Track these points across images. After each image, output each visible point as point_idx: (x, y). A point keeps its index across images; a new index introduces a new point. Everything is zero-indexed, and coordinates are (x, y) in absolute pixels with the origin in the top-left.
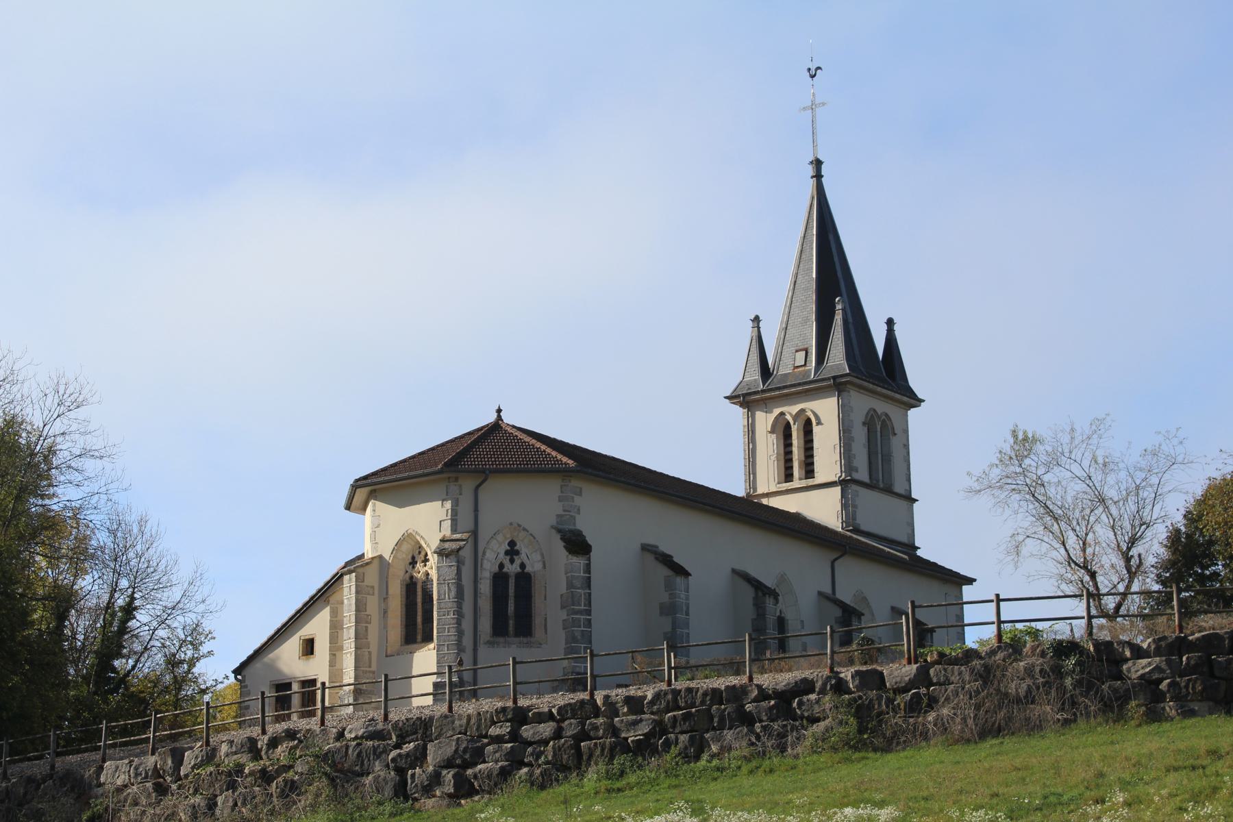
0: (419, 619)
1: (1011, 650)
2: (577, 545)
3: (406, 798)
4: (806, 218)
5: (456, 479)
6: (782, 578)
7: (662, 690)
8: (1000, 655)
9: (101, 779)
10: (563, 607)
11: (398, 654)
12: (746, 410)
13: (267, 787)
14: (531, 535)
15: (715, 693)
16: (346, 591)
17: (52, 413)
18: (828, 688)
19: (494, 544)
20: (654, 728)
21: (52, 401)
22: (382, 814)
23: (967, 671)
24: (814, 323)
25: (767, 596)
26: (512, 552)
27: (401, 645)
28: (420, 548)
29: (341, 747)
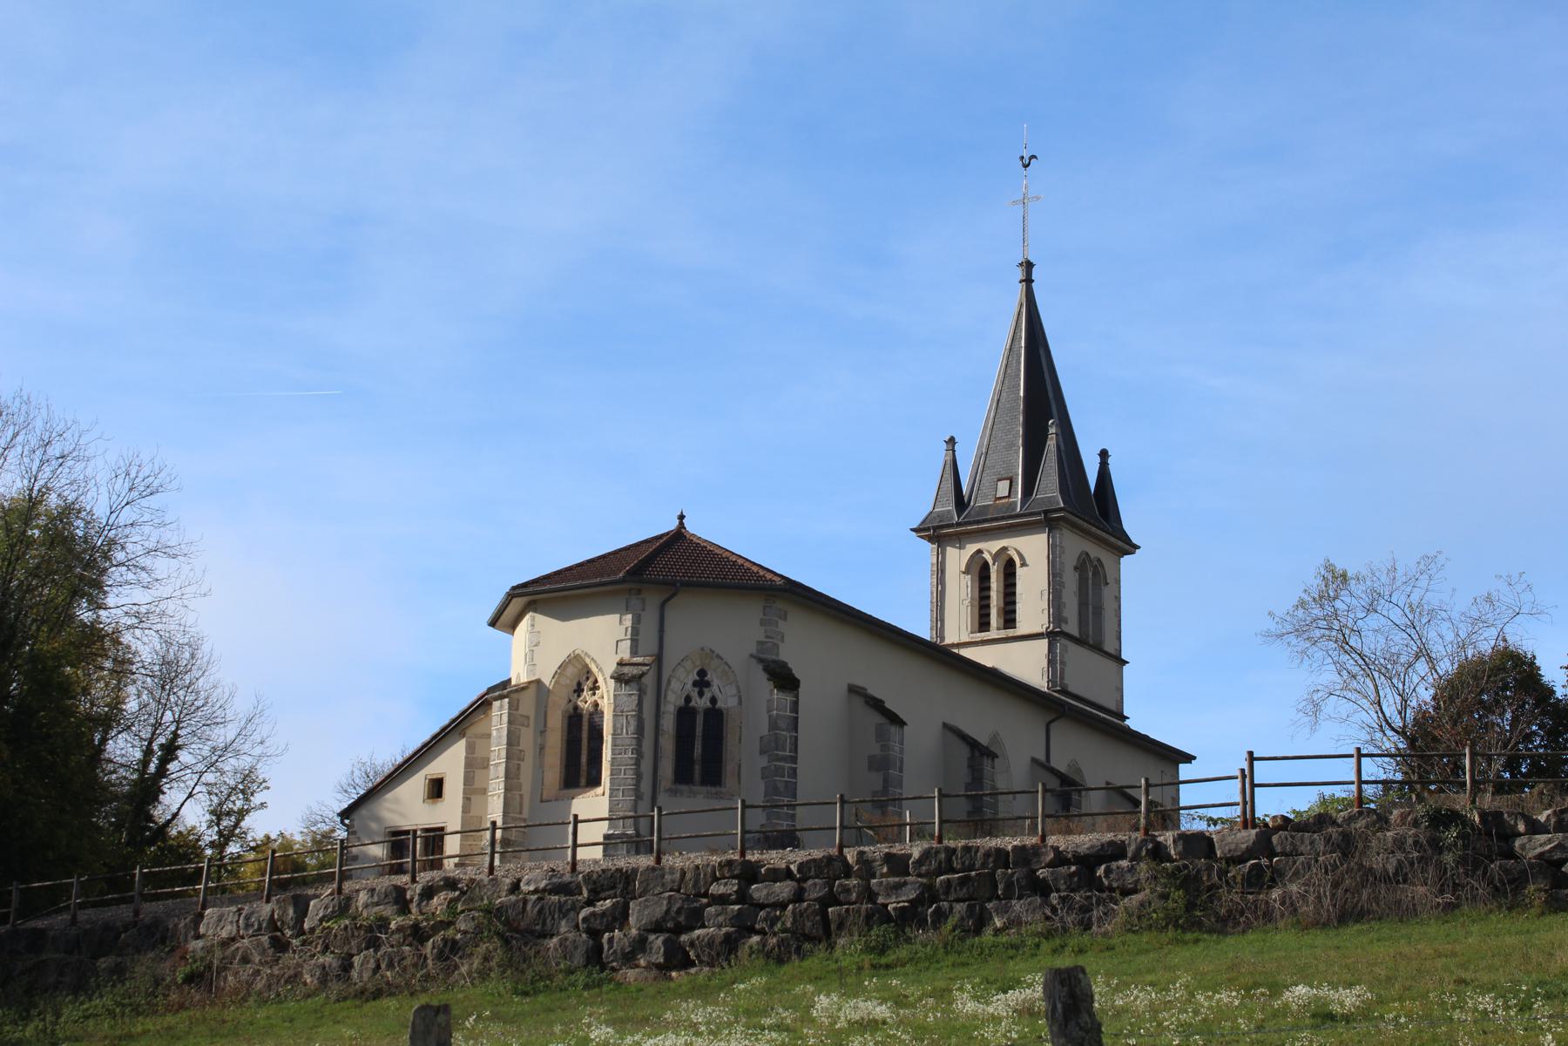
0: (584, 759)
1: (1375, 817)
2: (784, 679)
3: (603, 967)
4: (1013, 327)
5: (639, 592)
6: (995, 738)
7: (932, 848)
8: (1361, 824)
9: (201, 930)
10: (762, 752)
11: (556, 800)
12: (936, 546)
13: (420, 947)
14: (726, 664)
15: (1000, 854)
16: (495, 720)
17: (120, 499)
18: (1144, 853)
19: (681, 672)
20: (922, 893)
21: (121, 485)
22: (573, 985)
23: (1320, 839)
24: (1021, 449)
25: (985, 757)
26: (702, 683)
27: (560, 789)
28: (588, 672)
29: (517, 901)
